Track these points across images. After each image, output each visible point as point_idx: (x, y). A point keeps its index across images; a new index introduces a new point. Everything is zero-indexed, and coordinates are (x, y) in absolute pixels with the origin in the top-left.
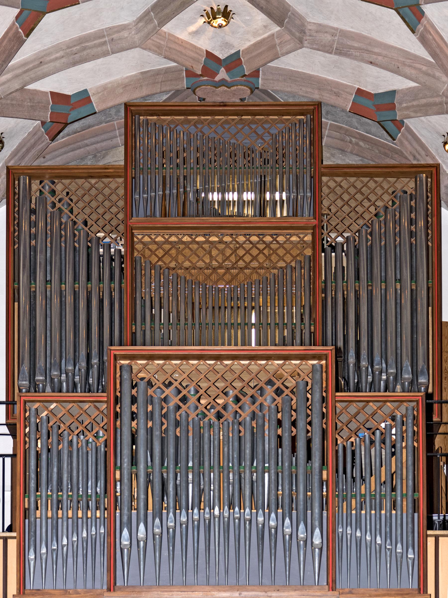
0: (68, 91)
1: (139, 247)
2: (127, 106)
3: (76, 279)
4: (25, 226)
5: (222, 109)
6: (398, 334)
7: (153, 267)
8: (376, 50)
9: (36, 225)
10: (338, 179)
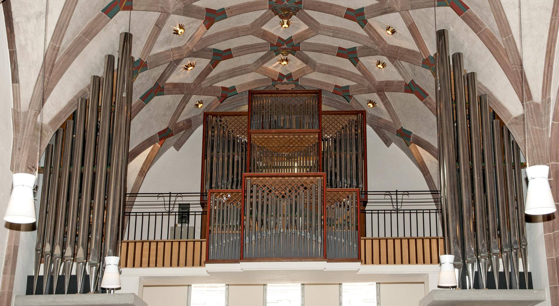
0: (228, 87)
1: (253, 139)
2: (249, 91)
3: (229, 151)
4: (210, 133)
5: (285, 92)
6: (351, 169)
7: (258, 147)
8: (342, 72)
9: (214, 132)
10: (328, 116)
